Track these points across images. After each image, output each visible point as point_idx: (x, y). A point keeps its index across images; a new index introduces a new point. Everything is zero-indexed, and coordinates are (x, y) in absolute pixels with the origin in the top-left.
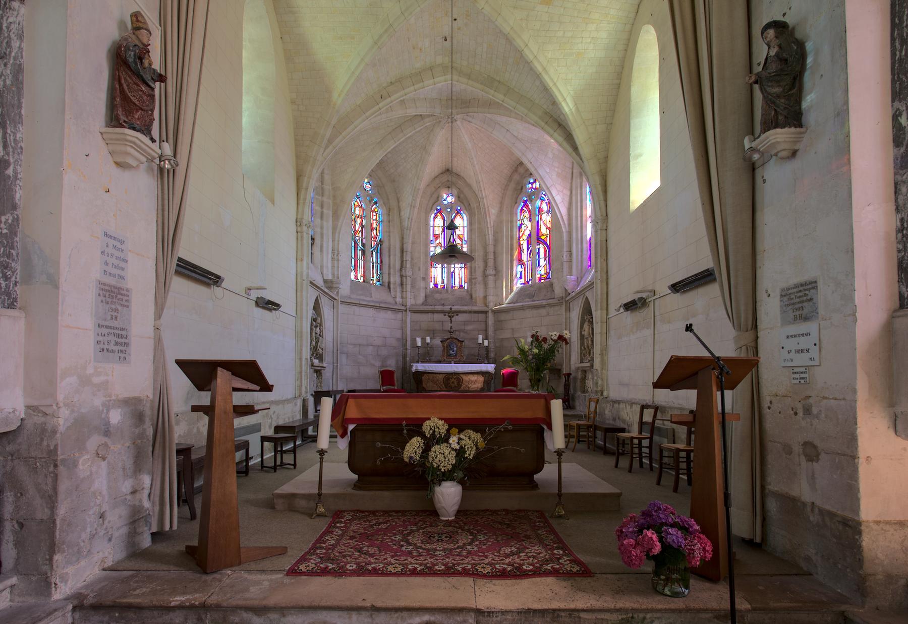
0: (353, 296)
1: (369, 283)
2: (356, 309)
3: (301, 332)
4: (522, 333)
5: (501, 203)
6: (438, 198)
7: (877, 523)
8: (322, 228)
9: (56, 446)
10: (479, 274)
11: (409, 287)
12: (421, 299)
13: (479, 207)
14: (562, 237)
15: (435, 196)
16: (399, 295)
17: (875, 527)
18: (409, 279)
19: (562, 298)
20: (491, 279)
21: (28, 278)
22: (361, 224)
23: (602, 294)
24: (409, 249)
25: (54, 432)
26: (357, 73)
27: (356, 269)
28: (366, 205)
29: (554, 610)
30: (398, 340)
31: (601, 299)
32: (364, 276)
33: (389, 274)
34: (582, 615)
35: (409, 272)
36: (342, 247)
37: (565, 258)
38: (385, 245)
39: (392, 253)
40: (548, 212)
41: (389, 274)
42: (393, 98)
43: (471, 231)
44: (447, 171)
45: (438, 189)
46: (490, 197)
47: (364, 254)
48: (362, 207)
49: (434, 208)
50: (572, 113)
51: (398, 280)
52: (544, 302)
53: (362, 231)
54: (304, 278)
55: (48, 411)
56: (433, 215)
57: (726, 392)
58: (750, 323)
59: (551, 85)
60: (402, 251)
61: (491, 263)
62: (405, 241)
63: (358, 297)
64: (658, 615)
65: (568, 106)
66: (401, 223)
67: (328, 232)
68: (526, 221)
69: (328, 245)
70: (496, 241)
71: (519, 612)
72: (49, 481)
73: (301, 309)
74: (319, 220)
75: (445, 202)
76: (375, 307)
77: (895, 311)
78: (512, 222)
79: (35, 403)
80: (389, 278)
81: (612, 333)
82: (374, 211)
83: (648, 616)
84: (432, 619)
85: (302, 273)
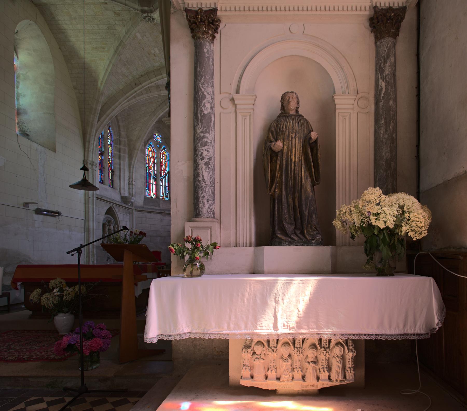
0: (145, 207)
2: (148, 215)
3: (89, 228)
8: (120, 165)
22: (154, 162)
26: (109, 70)
27: (149, 190)
28: (157, 150)
42: (143, 85)
47: (155, 180)
48: (154, 151)
53: (154, 166)
57: (77, 263)
63: (149, 207)
67: (127, 168)
73: (88, 215)
74: (118, 161)
82: (163, 154)
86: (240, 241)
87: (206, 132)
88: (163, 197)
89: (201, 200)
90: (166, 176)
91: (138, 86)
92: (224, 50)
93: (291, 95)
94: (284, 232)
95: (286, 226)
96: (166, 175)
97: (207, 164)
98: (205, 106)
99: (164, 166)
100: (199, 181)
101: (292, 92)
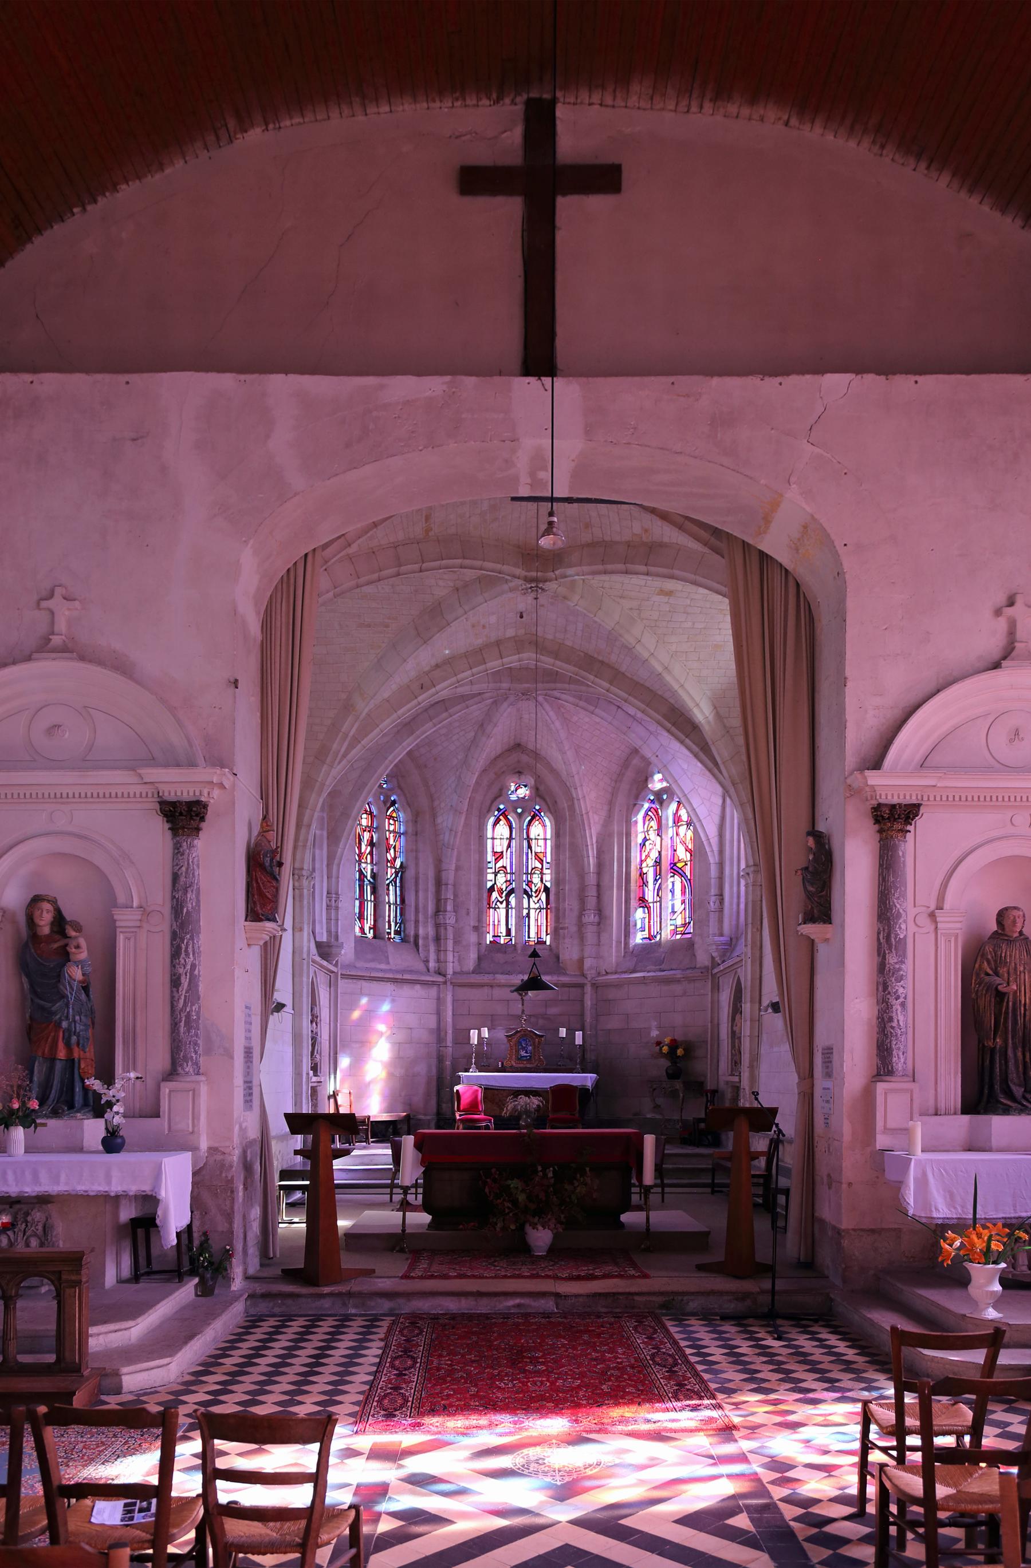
1: (383, 938)
4: (649, 1018)
5: (611, 803)
6: (501, 793)
7: (854, 1230)
9: (232, 1177)
10: (570, 922)
11: (450, 944)
12: (471, 962)
13: (572, 808)
14: (709, 870)
15: (495, 790)
16: (432, 957)
17: (852, 1232)
18: (450, 930)
19: (706, 968)
20: (590, 933)
21: (208, 1051)
22: (371, 843)
23: (752, 979)
24: (451, 881)
25: (231, 1167)
27: (361, 917)
28: (379, 809)
29: (614, 1294)
30: (431, 1031)
31: (752, 987)
32: (374, 927)
33: (417, 922)
34: (637, 1298)
35: (450, 919)
36: (343, 887)
37: (713, 906)
38: (410, 874)
39: (421, 887)
40: (689, 824)
41: (417, 922)
42: (438, 687)
43: (557, 847)
44: (517, 747)
45: (500, 775)
46: (590, 799)
47: (374, 891)
48: (371, 813)
49: (494, 807)
50: (709, 722)
51: (431, 931)
52: (678, 974)
54: (305, 956)
55: (227, 1151)
56: (492, 820)
58: (807, 1072)
59: (676, 687)
60: (439, 883)
61: (591, 902)
62: (444, 866)
64: (693, 1297)
65: (702, 713)
66: (437, 835)
67: (321, 865)
68: (652, 835)
69: (321, 885)
70: (600, 866)
71: (588, 1296)
72: (228, 1203)
75: (513, 797)
76: (394, 981)
77: (874, 1077)
78: (628, 835)
79: (216, 1145)
80: (417, 927)
81: (764, 1037)
82: (391, 817)
83: (685, 1298)
84: (522, 1301)
85: (302, 948)
86: (942, 1105)
87: (902, 962)
88: (389, 933)
89: (894, 1052)
90: (397, 876)
91: (428, 689)
92: (923, 848)
93: (1015, 913)
94: (1014, 1099)
95: (1014, 1088)
96: (397, 873)
97: (903, 1005)
98: (900, 928)
99: (392, 851)
100: (892, 1027)
101: (1015, 908)
